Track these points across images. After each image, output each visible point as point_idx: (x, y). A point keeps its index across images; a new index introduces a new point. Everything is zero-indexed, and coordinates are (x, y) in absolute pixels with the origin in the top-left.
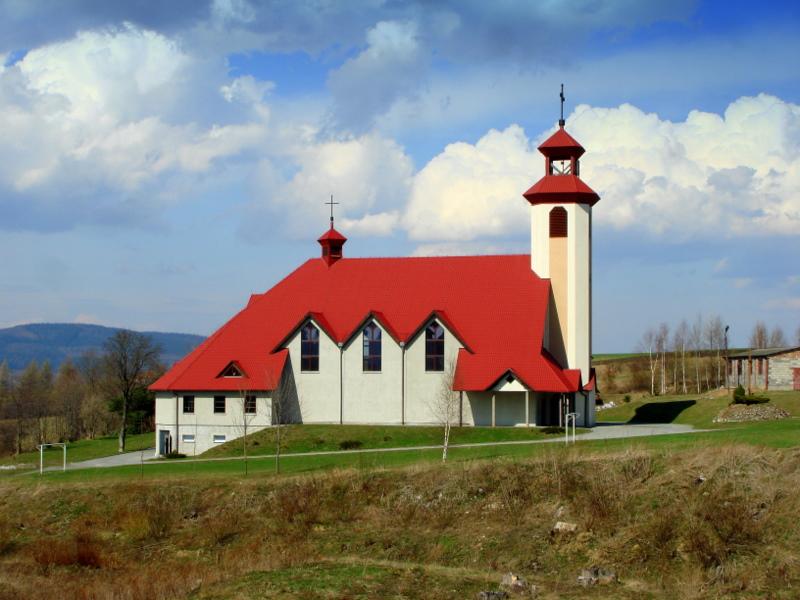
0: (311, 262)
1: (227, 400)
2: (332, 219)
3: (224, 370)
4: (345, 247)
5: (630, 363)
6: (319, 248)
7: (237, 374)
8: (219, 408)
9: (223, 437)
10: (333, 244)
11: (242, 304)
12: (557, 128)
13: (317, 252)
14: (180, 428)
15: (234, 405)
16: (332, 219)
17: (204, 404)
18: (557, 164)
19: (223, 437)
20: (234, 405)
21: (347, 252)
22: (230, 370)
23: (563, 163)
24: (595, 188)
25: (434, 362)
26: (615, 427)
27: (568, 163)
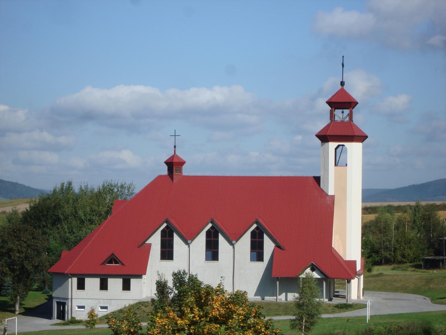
0: (160, 177)
1: (86, 279)
2: (175, 147)
3: (106, 260)
4: (184, 167)
5: (347, 119)
6: (166, 167)
7: (116, 263)
8: (104, 286)
9: (106, 308)
10: (173, 165)
11: (15, 182)
12: (340, 87)
13: (164, 171)
14: (73, 300)
15: (115, 284)
16: (175, 147)
17: (92, 283)
18: (338, 112)
19: (106, 308)
20: (115, 284)
21: (187, 171)
22: (112, 260)
23: (343, 112)
24: (367, 133)
25: (257, 251)
26: (234, 282)
27: (347, 112)
